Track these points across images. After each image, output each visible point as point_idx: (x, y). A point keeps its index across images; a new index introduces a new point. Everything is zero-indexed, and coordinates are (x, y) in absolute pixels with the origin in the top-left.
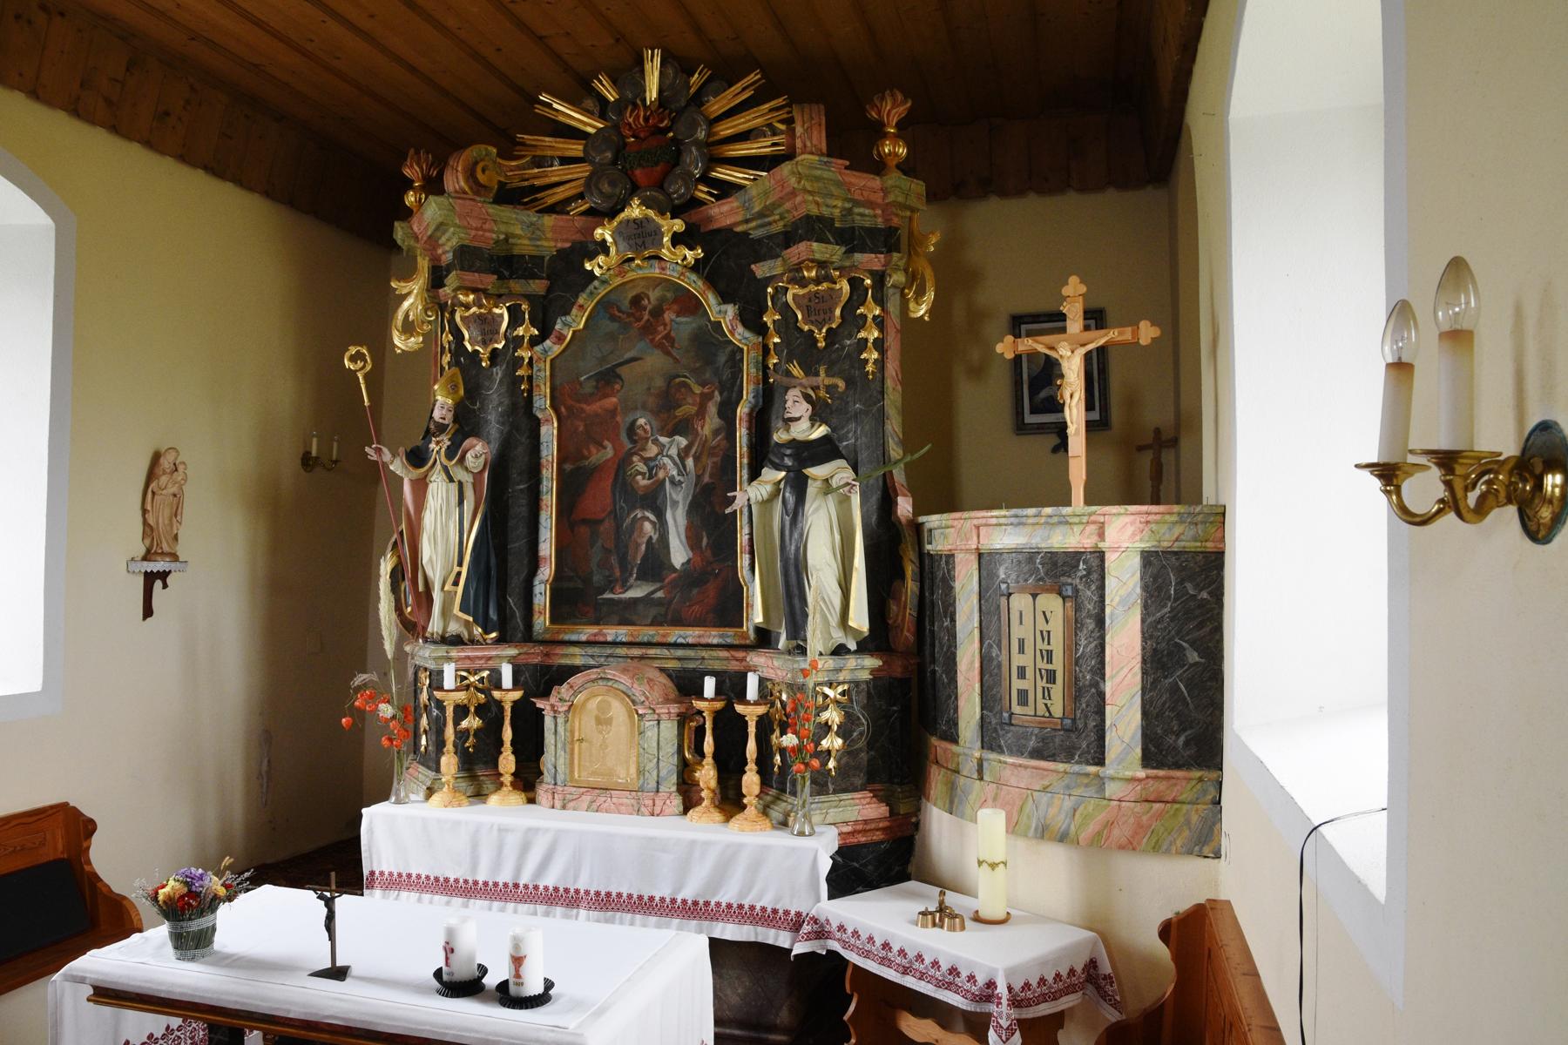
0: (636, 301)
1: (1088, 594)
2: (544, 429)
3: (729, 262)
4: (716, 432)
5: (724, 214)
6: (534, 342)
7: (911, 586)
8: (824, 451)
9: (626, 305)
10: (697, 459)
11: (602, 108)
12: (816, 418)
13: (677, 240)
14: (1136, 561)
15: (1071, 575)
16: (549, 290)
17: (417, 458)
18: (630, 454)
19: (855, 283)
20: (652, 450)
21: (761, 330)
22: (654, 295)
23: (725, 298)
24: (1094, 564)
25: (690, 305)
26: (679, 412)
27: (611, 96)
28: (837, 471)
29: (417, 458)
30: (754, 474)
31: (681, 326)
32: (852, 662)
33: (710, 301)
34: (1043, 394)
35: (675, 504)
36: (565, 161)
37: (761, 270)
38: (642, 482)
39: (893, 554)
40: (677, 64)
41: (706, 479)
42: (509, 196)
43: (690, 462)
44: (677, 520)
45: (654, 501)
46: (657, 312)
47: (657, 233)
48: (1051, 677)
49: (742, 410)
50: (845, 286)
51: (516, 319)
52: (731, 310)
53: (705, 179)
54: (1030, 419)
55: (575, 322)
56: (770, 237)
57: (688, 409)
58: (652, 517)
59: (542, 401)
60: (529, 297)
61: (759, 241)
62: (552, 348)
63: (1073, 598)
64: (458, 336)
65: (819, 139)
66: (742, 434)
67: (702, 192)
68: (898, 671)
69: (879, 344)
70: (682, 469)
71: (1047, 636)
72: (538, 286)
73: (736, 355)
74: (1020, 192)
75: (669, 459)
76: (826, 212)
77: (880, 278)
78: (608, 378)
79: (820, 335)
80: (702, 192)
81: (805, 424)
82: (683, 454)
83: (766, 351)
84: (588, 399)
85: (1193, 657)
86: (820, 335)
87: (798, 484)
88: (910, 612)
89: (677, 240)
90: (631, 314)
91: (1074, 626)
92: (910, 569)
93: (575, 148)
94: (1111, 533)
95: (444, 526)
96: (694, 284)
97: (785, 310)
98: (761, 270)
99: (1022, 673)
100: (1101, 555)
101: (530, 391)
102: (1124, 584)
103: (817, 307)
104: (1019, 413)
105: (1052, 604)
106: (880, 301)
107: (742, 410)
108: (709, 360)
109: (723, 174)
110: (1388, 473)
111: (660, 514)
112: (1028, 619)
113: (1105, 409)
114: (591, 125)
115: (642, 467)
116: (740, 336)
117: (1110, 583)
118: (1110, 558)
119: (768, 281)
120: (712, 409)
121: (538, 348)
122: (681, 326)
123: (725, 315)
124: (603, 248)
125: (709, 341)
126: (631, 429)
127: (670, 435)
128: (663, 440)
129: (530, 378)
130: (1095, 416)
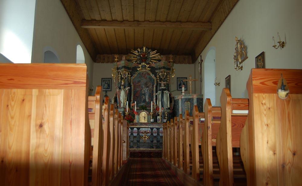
0: (143, 73)
1: (192, 102)
2: (132, 86)
3: (153, 70)
4: (151, 88)
5: (153, 65)
6: (130, 77)
7: (173, 103)
8: (165, 90)
9: (141, 73)
10: (149, 90)
11: (138, 52)
12: (164, 86)
13: (148, 67)
14: (196, 99)
15: (190, 100)
16: (132, 71)
17: (120, 88)
18: (141, 90)
19: (167, 73)
20: (144, 89)
21: (157, 77)
22: (145, 73)
23: (153, 74)
24: (192, 99)
25: (149, 74)
26: (147, 85)
27: (140, 51)
28: (166, 92)
29: (120, 88)
30: (156, 92)
31: (148, 77)
32: (168, 110)
33: (151, 75)
34: (180, 86)
35: (147, 95)
36: (134, 57)
37: (156, 71)
38: (143, 93)
39: (171, 99)
40: (148, 48)
41: (150, 92)
42: (129, 60)
43: (149, 91)
44: (147, 97)
45: (144, 94)
46: (145, 75)
47: (146, 66)
48: (189, 109)
49: (155, 86)
50: (166, 73)
51: (128, 74)
52: (154, 75)
53: (150, 61)
54: (179, 89)
55: (135, 75)
56: (158, 68)
57: (149, 85)
58: (144, 96)
59: (132, 84)
60: (130, 72)
61: (156, 68)
62: (133, 78)
63: (191, 102)
64: (121, 76)
65: (165, 59)
66: (155, 88)
67: (150, 62)
68: (171, 112)
69: (169, 79)
70: (148, 91)
71: (188, 105)
72: (131, 71)
73: (154, 80)
74: (178, 64)
75: (146, 90)
76: (165, 66)
77: (169, 73)
78: (139, 82)
79: (163, 78)
80: (150, 62)
81: (163, 87)
82: (148, 90)
83: (157, 80)
84: (137, 83)
85: (201, 107)
86: (163, 78)
87: (163, 93)
88: (173, 106)
89: (148, 67)
90: (142, 75)
91: (191, 104)
92: (173, 101)
93: (136, 56)
94: (194, 97)
95: (122, 96)
96: (149, 72)
97: (160, 76)
98: (156, 71)
99: (186, 109)
100: (193, 98)
101: (130, 82)
102: (195, 101)
103: (163, 75)
104: (178, 88)
105: (189, 103)
106: (169, 75)
107: (155, 86)
108: (151, 80)
109: (152, 61)
110: (215, 84)
111: (145, 96)
112: (187, 104)
113: (187, 88)
114: (137, 54)
115: (143, 91)
116: (155, 78)
117: (194, 101)
118: (194, 98)
119: (157, 73)
120: (151, 85)
121: (131, 78)
122: (148, 77)
123: (153, 76)
124: (140, 67)
125: (151, 79)
126: (142, 87)
127: (146, 88)
128: (146, 88)
129: (130, 81)
130: (186, 89)
